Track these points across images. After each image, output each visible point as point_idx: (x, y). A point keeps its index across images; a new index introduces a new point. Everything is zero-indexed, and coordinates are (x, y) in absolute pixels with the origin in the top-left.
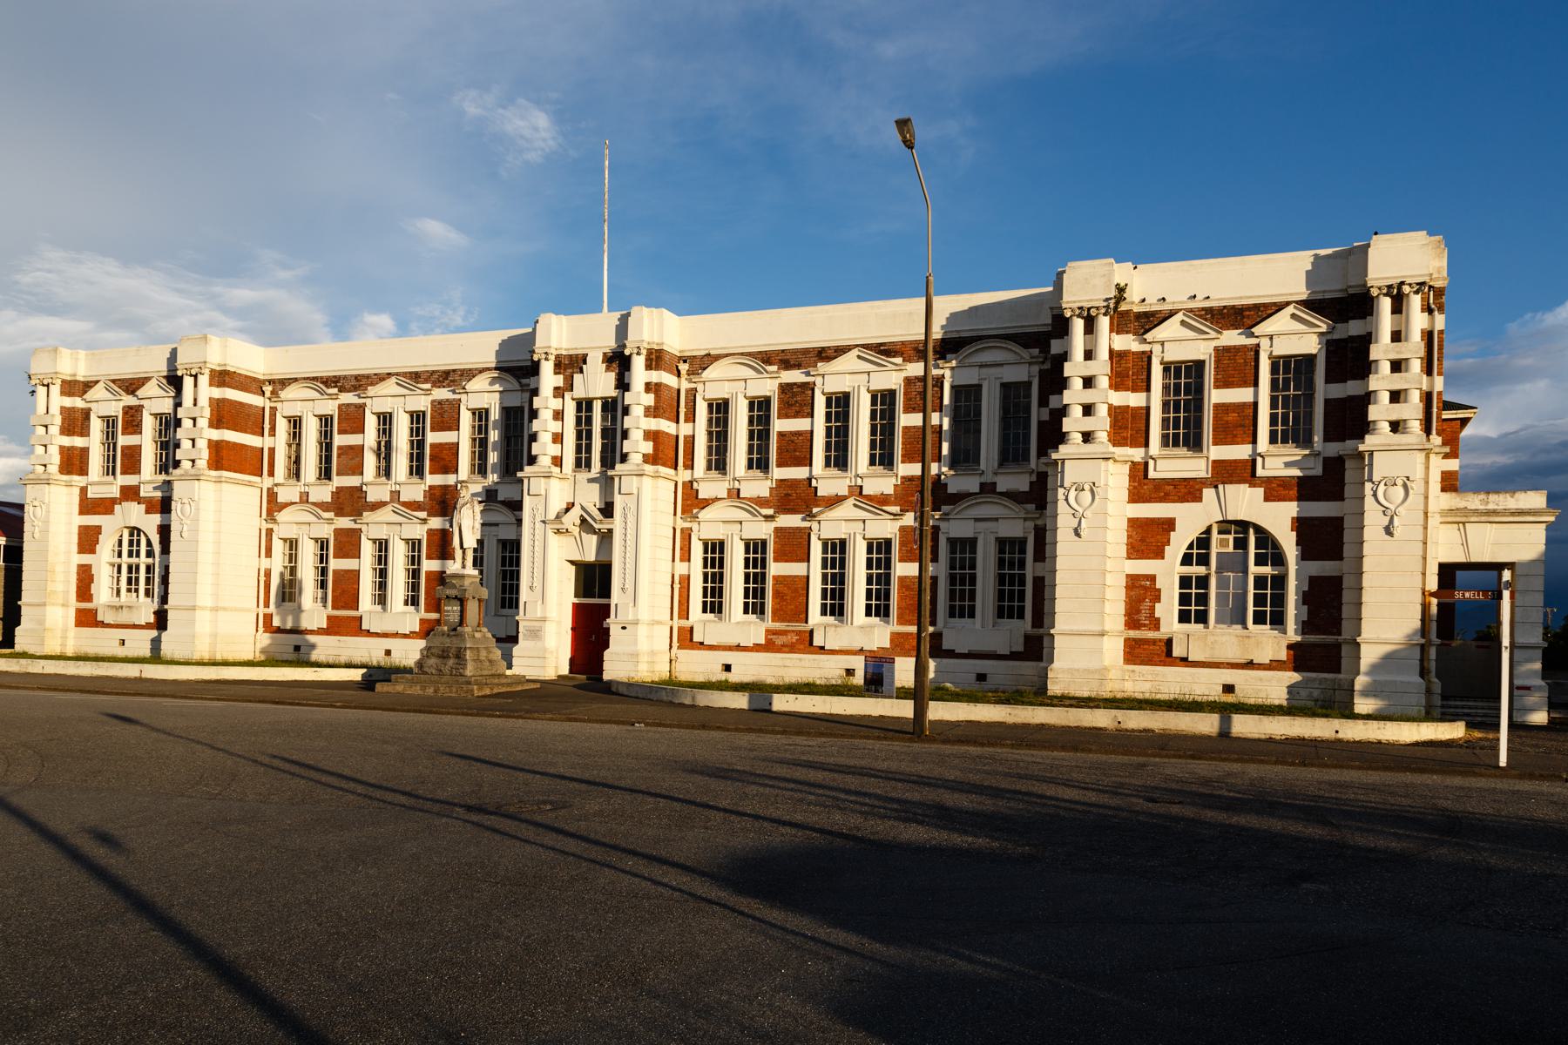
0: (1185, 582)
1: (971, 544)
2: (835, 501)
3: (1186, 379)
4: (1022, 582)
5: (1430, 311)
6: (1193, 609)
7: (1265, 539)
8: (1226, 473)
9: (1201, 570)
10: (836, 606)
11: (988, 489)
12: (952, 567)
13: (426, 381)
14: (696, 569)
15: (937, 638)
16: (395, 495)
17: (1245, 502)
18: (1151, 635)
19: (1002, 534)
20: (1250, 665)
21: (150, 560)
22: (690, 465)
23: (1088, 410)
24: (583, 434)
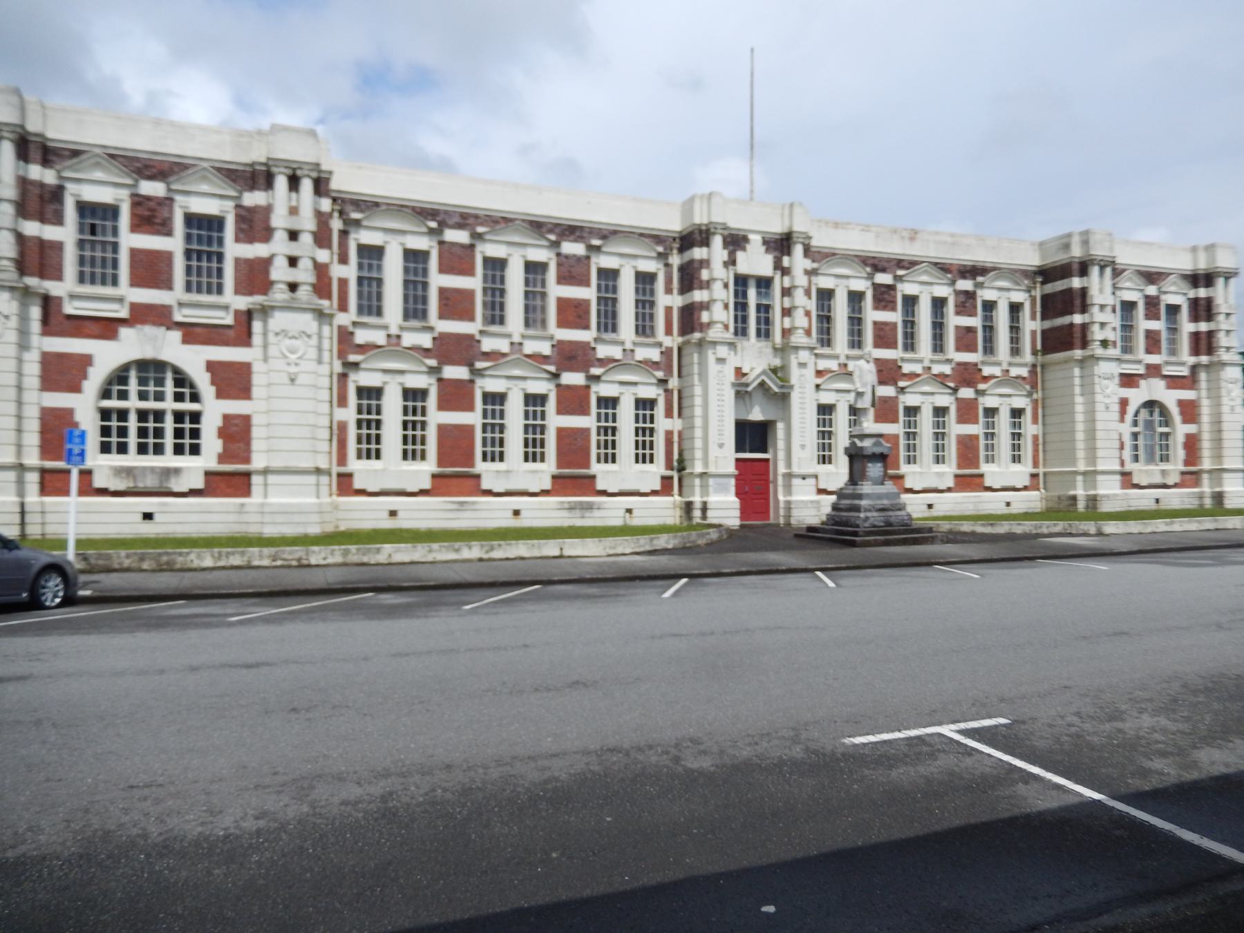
2: (913, 375)
3: (204, 228)
7: (181, 380)
8: (142, 315)
13: (551, 231)
14: (349, 415)
19: (938, 404)
21: (1191, 428)
23: (293, 262)
24: (741, 306)
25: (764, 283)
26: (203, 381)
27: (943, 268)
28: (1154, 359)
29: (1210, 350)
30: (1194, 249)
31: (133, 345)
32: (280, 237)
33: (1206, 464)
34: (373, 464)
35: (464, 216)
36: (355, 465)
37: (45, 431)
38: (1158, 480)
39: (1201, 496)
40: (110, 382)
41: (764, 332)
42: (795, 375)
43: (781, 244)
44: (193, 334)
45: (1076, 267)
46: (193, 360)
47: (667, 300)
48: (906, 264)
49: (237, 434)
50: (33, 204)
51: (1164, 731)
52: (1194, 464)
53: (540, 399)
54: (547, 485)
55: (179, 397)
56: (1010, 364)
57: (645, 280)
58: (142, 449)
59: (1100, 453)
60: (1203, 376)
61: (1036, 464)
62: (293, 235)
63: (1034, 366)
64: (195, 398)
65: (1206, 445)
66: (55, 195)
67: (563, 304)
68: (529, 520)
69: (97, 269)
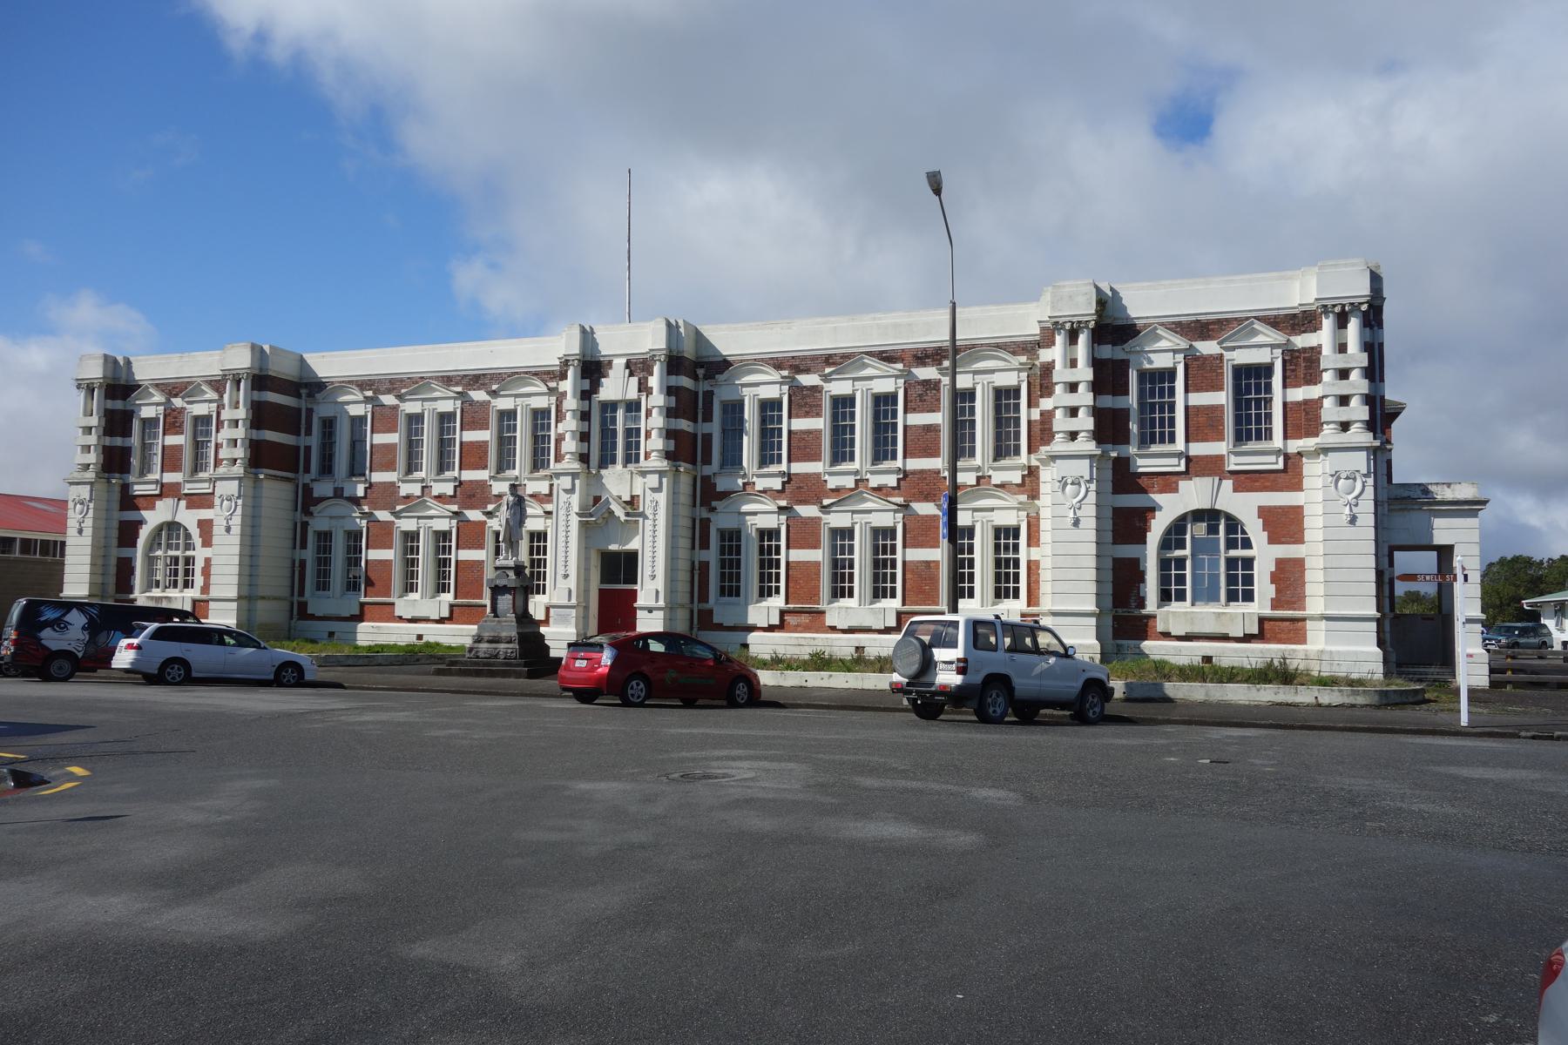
1: (848, 533)
3: (1251, 379)
4: (1017, 565)
5: (1371, 327)
7: (1233, 524)
8: (1195, 467)
9: (1233, 553)
12: (722, 553)
13: (457, 384)
15: (303, 606)
20: (1225, 638)
22: (707, 460)
25: (633, 407)
26: (1255, 529)
28: (170, 477)
31: (1194, 494)
35: (392, 381)
37: (118, 566)
40: (1168, 532)
44: (1247, 481)
46: (1245, 506)
48: (838, 359)
49: (1289, 577)
52: (1291, 605)
55: (1231, 544)
64: (1247, 544)
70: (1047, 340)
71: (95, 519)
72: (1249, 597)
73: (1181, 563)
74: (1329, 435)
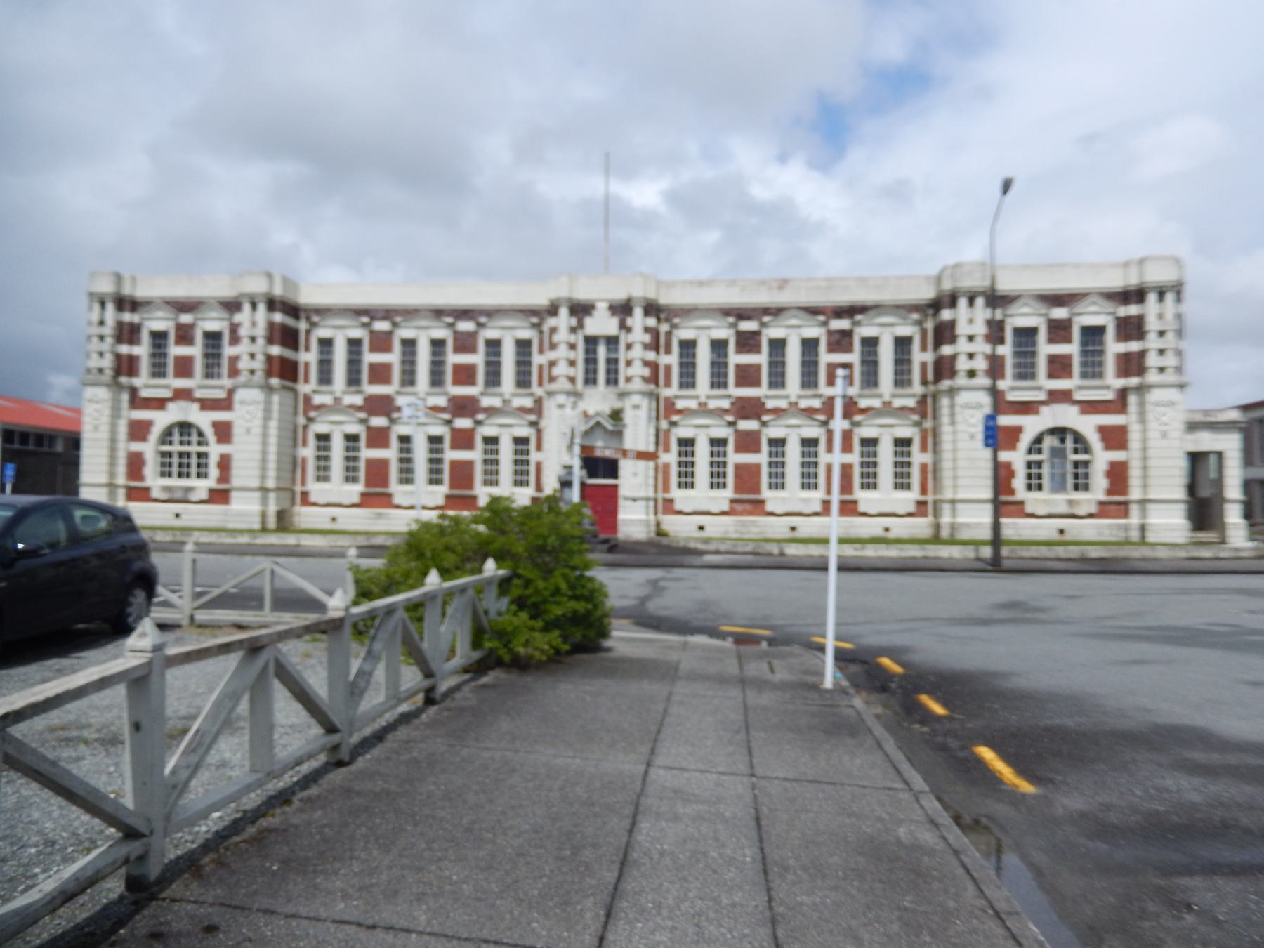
0: (1029, 465)
6: (1034, 483)
7: (1078, 438)
8: (1058, 397)
10: (407, 477)
11: (887, 404)
15: (669, 502)
16: (337, 400)
17: (1067, 416)
18: (1010, 498)
24: (591, 361)
25: (612, 341)
27: (813, 311)
29: (1141, 370)
30: (1126, 265)
32: (246, 341)
33: (1135, 493)
34: (689, 492)
36: (676, 493)
38: (1063, 509)
39: (1126, 528)
41: (612, 380)
42: (628, 416)
43: (622, 309)
44: (1090, 407)
45: (947, 300)
46: (1088, 425)
47: (921, 357)
49: (1118, 474)
50: (126, 335)
51: (1163, 777)
53: (721, 442)
54: (726, 507)
56: (894, 396)
57: (902, 344)
58: (180, 475)
59: (961, 482)
60: (1132, 399)
61: (924, 490)
62: (253, 339)
63: (924, 397)
64: (1087, 450)
65: (1134, 474)
66: (847, 335)
67: (373, 367)
68: (803, 532)
69: (158, 370)
70: (553, 310)
71: (280, 420)
72: (206, 476)
73: (1039, 464)
74: (961, 380)
